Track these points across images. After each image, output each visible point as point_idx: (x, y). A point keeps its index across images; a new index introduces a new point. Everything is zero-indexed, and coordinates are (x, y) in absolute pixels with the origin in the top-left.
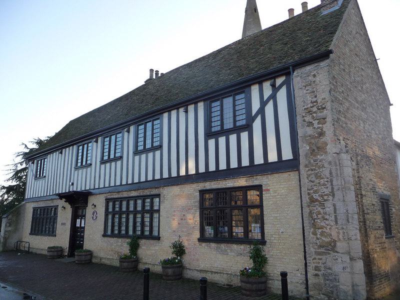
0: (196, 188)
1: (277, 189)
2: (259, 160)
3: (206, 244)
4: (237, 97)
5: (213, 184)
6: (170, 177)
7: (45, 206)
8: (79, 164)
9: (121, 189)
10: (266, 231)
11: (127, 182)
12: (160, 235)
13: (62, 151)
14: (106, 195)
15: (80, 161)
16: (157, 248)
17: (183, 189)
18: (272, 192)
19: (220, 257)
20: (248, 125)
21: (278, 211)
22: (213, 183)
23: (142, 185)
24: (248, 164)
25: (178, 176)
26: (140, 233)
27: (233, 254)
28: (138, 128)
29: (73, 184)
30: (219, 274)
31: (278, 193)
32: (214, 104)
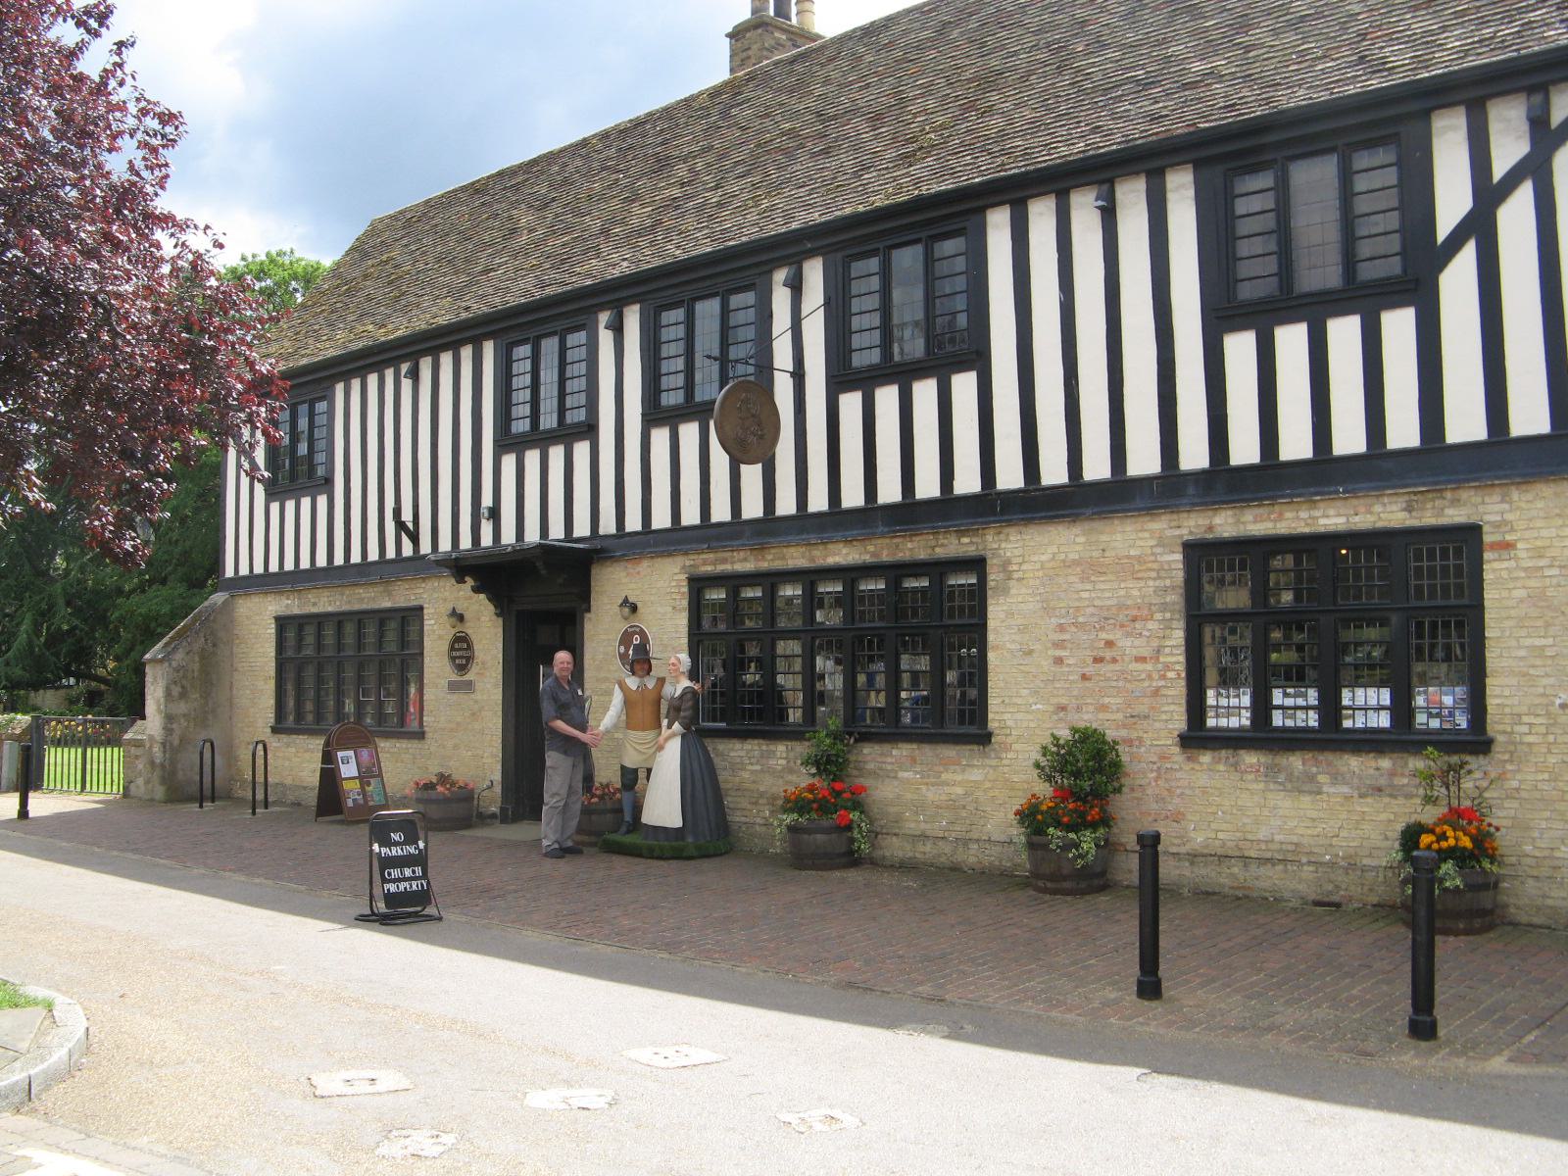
0: (1169, 533)
2: (1054, 471)
4: (1362, 160)
10: (1492, 703)
12: (1495, 725)
16: (976, 775)
17: (1104, 538)
18: (1522, 554)
20: (589, 425)
21: (1547, 625)
22: (1248, 515)
24: (638, 527)
25: (417, 557)
26: (1246, 722)
27: (1345, 789)
28: (846, 268)
30: (1280, 867)
31: (1554, 558)
32: (858, 268)
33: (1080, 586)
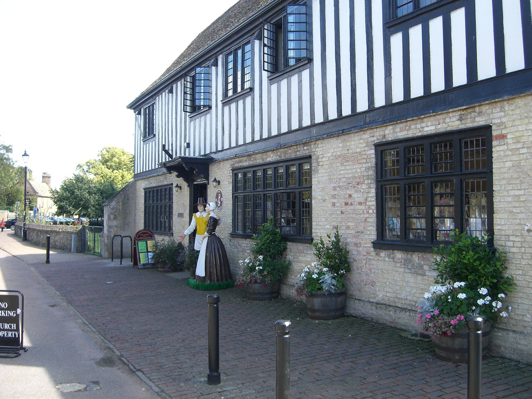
1: (521, 134)
3: (387, 252)
5: (398, 130)
6: (389, 105)
7: (158, 185)
8: (230, 93)
9: (252, 148)
11: (261, 136)
13: (172, 87)
14: (231, 162)
15: (230, 86)
17: (348, 144)
18: (510, 141)
19: (410, 278)
21: (522, 183)
22: (398, 127)
23: (314, 131)
29: (188, 145)
33: (340, 168)
